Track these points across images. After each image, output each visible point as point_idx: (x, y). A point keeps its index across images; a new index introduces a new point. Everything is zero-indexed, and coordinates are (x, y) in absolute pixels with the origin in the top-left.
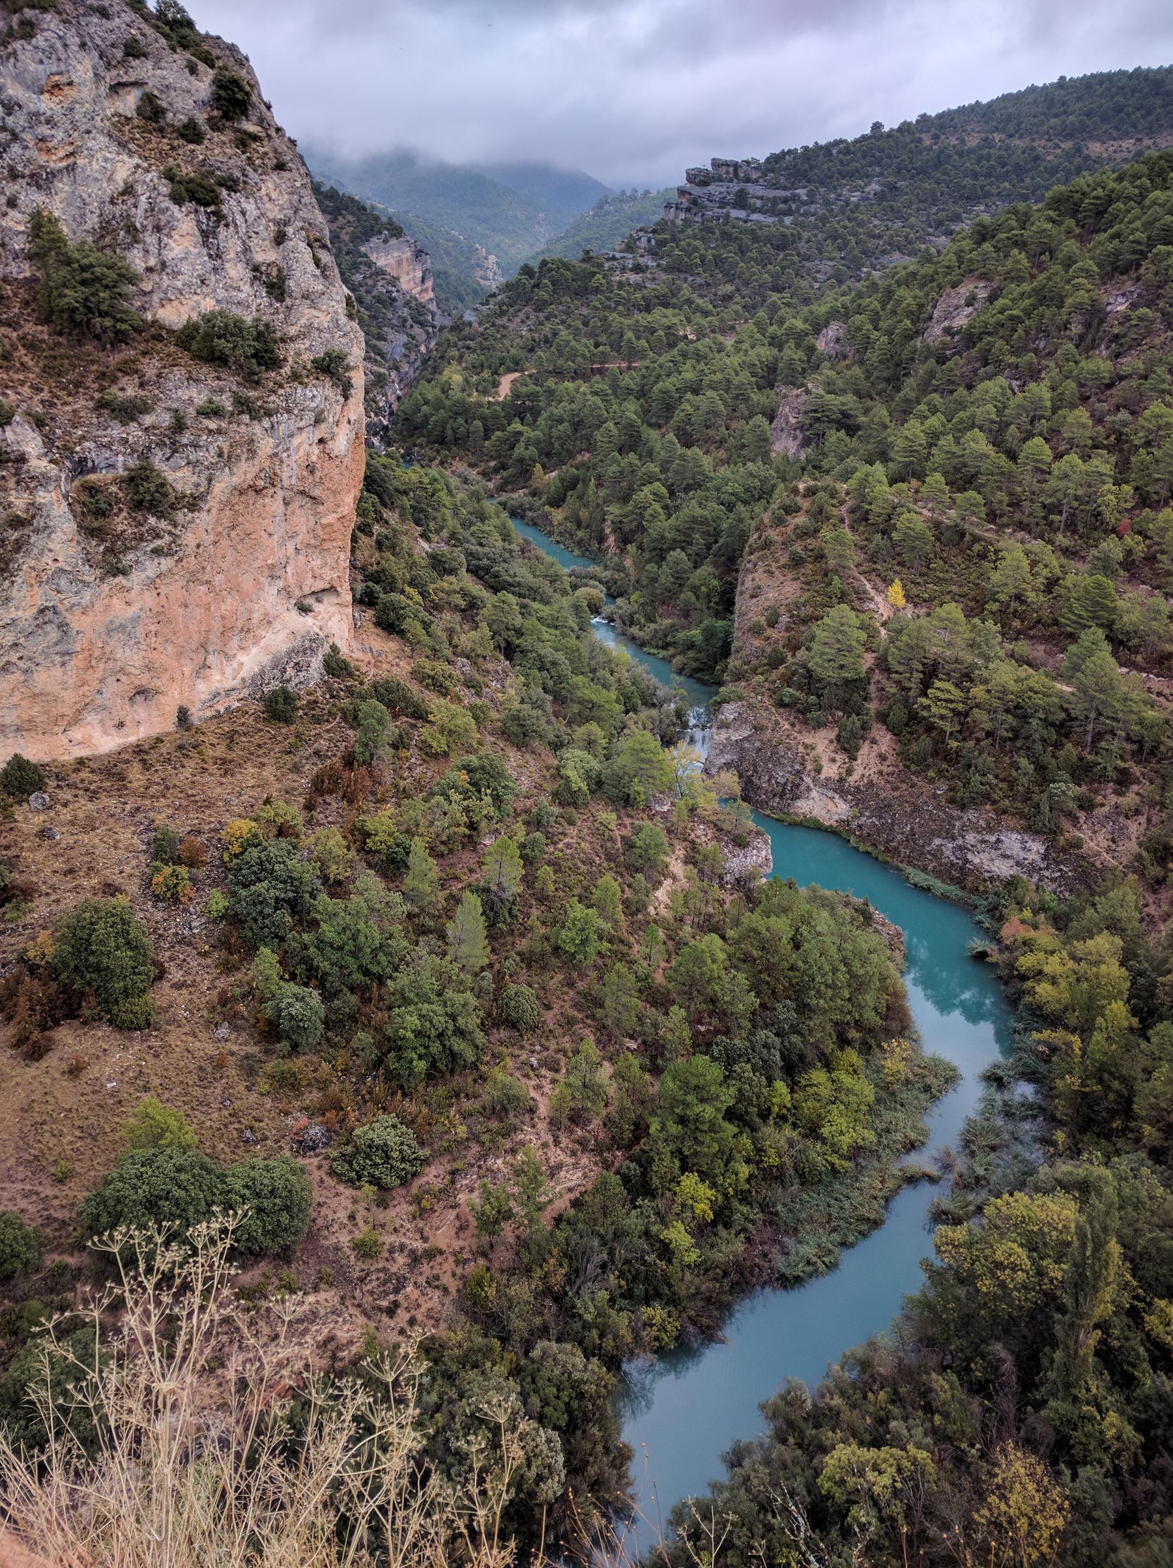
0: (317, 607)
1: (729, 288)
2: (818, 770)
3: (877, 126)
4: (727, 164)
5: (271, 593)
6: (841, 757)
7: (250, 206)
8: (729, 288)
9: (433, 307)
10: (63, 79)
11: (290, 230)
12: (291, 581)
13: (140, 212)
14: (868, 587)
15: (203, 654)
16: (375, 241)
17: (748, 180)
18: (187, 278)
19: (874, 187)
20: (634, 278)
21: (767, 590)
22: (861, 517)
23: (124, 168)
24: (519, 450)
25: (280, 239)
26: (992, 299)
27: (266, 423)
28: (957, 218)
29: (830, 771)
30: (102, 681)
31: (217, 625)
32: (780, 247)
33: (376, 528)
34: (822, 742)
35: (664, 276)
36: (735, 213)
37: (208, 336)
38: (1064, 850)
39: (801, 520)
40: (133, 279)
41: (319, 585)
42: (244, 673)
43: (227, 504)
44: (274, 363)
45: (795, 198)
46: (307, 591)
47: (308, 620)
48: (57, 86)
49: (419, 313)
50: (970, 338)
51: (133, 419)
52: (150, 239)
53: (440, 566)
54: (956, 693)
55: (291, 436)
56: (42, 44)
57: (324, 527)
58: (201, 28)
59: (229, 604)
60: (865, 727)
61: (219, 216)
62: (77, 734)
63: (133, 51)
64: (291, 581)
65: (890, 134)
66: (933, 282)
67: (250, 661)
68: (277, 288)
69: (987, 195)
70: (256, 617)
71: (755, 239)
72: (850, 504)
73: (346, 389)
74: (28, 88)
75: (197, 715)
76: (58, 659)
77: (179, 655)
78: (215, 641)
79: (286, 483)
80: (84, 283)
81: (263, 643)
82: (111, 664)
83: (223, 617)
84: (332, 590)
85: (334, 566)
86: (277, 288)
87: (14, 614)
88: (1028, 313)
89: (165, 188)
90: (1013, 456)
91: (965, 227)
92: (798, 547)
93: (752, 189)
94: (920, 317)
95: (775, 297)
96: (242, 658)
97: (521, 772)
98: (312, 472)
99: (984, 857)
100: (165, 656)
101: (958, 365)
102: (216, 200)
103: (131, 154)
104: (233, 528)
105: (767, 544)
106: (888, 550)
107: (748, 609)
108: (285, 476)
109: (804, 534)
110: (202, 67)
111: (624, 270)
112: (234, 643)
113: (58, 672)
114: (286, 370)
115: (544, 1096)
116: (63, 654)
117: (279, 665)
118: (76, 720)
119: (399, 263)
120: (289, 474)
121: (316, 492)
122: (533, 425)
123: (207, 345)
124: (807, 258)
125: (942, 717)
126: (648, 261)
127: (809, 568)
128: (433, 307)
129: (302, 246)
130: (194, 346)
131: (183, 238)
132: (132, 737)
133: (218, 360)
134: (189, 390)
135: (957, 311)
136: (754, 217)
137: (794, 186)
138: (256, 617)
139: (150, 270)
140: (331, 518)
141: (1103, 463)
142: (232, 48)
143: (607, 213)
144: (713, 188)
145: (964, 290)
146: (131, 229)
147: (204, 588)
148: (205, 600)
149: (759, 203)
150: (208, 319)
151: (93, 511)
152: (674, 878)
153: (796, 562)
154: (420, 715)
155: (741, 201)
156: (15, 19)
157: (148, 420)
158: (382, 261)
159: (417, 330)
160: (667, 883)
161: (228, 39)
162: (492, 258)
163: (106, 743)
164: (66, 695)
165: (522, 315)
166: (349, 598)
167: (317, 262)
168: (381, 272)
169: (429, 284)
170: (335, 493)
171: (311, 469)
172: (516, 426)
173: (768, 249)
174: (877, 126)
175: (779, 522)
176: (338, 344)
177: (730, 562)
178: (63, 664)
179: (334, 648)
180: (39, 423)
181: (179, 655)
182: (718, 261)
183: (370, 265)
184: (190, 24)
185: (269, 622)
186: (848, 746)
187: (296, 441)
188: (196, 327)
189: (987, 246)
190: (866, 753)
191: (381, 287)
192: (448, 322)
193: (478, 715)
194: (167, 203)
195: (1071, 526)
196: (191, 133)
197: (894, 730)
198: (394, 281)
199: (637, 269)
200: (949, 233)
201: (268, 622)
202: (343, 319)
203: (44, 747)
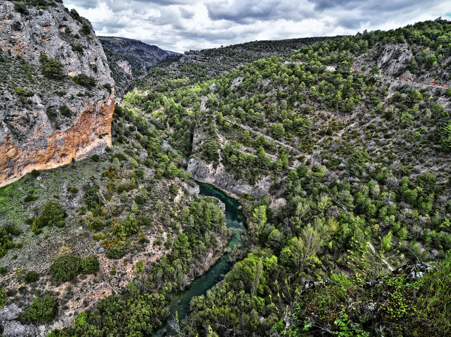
0: (103, 137)
1: (193, 75)
2: (209, 172)
3: (222, 46)
4: (193, 51)
5: (93, 134)
6: (214, 170)
7: (89, 52)
8: (193, 75)
9: (131, 76)
10: (49, 24)
11: (98, 58)
12: (98, 132)
13: (65, 52)
14: (219, 136)
15: (77, 146)
16: (119, 61)
17: (196, 54)
18: (73, 67)
19: (221, 58)
20: (173, 72)
21: (198, 136)
22: (218, 122)
23: (62, 43)
24: (149, 106)
25: (96, 59)
26: (244, 80)
27: (92, 98)
28: (237, 65)
29: (211, 172)
30: (54, 152)
31: (81, 141)
32: (203, 68)
33: (118, 121)
34: (210, 166)
35: (180, 72)
36: (194, 61)
37: (80, 79)
38: (255, 188)
39: (206, 122)
40: (63, 66)
41: (104, 133)
42: (87, 151)
43: (83, 115)
44: (95, 85)
45: (206, 59)
46: (101, 134)
47: (102, 140)
48: (47, 25)
49: (128, 77)
50: (239, 88)
51: (62, 96)
52: (67, 58)
53: (132, 129)
54: (236, 157)
55: (98, 101)
56: (44, 17)
57: (105, 120)
58: (80, 15)
59: (84, 136)
60: (218, 164)
61: (83, 54)
62: (48, 164)
63: (65, 19)
64: (98, 132)
65: (224, 48)
66: (233, 77)
67: (88, 148)
68: (95, 69)
69: (242, 61)
70: (90, 139)
71: (198, 66)
72: (215, 119)
73: (110, 92)
74: (40, 25)
75: (76, 160)
76: (44, 148)
77: (72, 147)
78: (81, 145)
79: (97, 111)
80: (51, 66)
81: (91, 145)
82: (56, 149)
83: (82, 139)
84: (107, 134)
85: (108, 129)
86: (95, 69)
87: (34, 137)
88: (250, 84)
89: (70, 47)
90: (247, 111)
91: (238, 67)
92: (205, 128)
93: (197, 56)
94: (230, 84)
95: (202, 78)
96: (87, 148)
97: (148, 173)
98: (103, 109)
99: (241, 189)
100: (70, 148)
101: (237, 94)
102: (82, 51)
103: (63, 40)
104: (85, 120)
105: (199, 127)
106: (224, 130)
107: (195, 139)
108: (97, 109)
109: (206, 125)
110: (80, 23)
111: (171, 71)
112: (85, 145)
113: (44, 150)
114: (97, 87)
115: (152, 240)
116: (45, 146)
117: (94, 149)
118: (48, 161)
119: (124, 66)
120: (98, 109)
121: (104, 113)
122: (153, 101)
123: (81, 81)
124: (208, 70)
125: (233, 162)
126: (176, 69)
127: (207, 132)
128: (131, 76)
129: (101, 61)
130: (77, 81)
131: (74, 60)
132: (62, 164)
133: (82, 84)
134: (73, 91)
135: (237, 82)
136: (198, 62)
137: (206, 56)
138: (90, 139)
139: (67, 64)
140: (107, 119)
141: (263, 113)
142: (87, 20)
143: (169, 59)
144: (190, 55)
145: (238, 79)
146: (63, 55)
147: (78, 133)
148: (78, 135)
149: (199, 59)
150: (80, 75)
151: (51, 115)
152: (179, 194)
153: (205, 131)
154: (125, 159)
155: (195, 59)
156: (38, 11)
157: (65, 96)
158: (121, 65)
159: (128, 80)
160: (178, 195)
161: (86, 18)
162: (144, 67)
163: (55, 166)
164: (46, 155)
165: (150, 78)
166: (111, 135)
167: (104, 65)
168: (120, 68)
169: (131, 71)
170: (107, 113)
171: (102, 108)
172: (149, 101)
173: (201, 68)
174: (222, 46)
175: (201, 123)
176: (109, 82)
177: (192, 130)
178: (45, 149)
179: (107, 146)
180: (41, 96)
181: (72, 147)
182: (191, 70)
183: (118, 66)
184: (78, 15)
185: (93, 141)
186: (215, 167)
187: (99, 102)
188: (77, 77)
189: (242, 71)
190: (218, 169)
191: (120, 71)
192: (134, 79)
193: (138, 161)
194: (71, 51)
195: (258, 125)
196: (77, 37)
197: (224, 164)
198: (123, 70)
199: (174, 70)
200: (235, 68)
201: (93, 140)
202: (110, 77)
203: (40, 167)
